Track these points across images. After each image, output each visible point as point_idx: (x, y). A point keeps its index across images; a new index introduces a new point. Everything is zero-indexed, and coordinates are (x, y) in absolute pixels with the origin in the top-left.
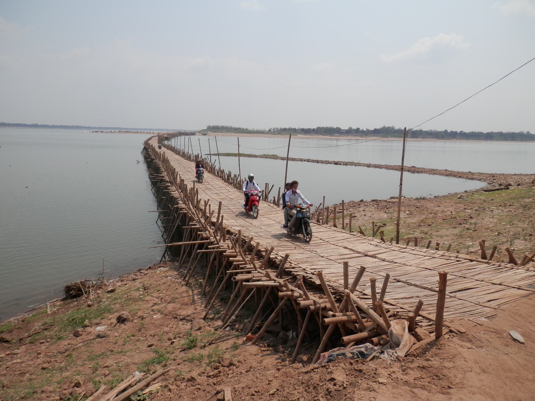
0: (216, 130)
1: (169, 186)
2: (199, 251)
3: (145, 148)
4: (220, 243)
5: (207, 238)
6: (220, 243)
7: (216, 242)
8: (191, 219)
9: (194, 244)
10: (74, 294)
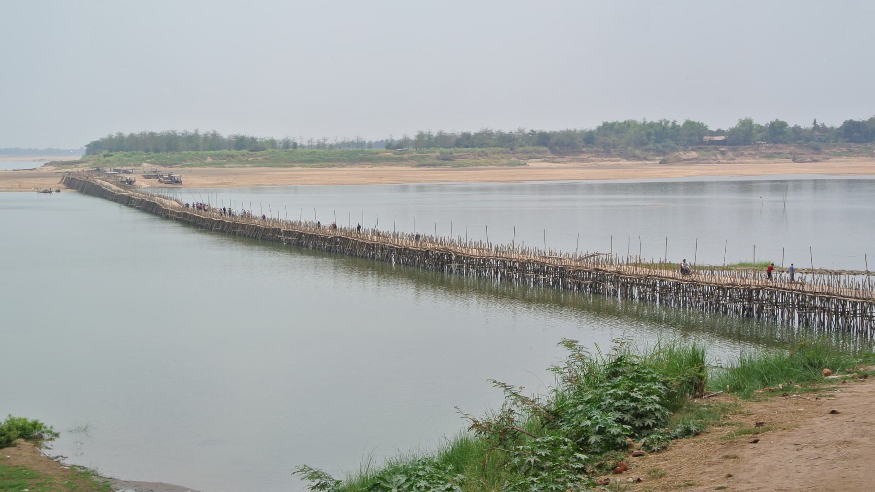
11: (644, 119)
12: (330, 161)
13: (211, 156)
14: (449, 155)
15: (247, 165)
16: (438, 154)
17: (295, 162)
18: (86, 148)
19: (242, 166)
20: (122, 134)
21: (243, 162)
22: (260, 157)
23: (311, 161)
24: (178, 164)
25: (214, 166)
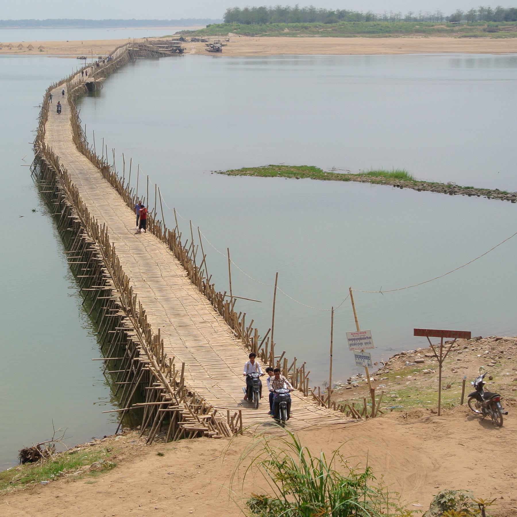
0: (257, 27)
1: (123, 318)
2: (106, 315)
3: (38, 160)
4: (180, 404)
5: (171, 399)
6: (180, 404)
7: (176, 404)
8: (155, 378)
9: (159, 405)
10: (31, 458)
11: (297, 6)
12: (389, 32)
13: (288, 27)
14: (494, 28)
15: (315, 35)
16: (486, 27)
17: (358, 33)
18: (224, 19)
19: (312, 36)
20: (238, 8)
21: (314, 32)
22: (330, 28)
23: (373, 32)
24: (259, 34)
25: (288, 36)
